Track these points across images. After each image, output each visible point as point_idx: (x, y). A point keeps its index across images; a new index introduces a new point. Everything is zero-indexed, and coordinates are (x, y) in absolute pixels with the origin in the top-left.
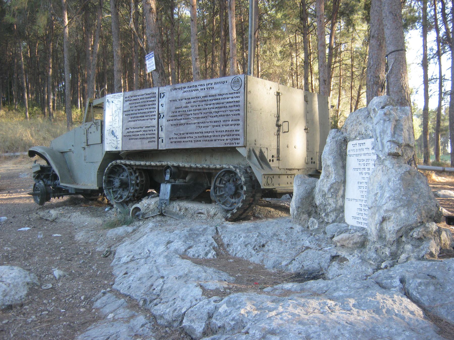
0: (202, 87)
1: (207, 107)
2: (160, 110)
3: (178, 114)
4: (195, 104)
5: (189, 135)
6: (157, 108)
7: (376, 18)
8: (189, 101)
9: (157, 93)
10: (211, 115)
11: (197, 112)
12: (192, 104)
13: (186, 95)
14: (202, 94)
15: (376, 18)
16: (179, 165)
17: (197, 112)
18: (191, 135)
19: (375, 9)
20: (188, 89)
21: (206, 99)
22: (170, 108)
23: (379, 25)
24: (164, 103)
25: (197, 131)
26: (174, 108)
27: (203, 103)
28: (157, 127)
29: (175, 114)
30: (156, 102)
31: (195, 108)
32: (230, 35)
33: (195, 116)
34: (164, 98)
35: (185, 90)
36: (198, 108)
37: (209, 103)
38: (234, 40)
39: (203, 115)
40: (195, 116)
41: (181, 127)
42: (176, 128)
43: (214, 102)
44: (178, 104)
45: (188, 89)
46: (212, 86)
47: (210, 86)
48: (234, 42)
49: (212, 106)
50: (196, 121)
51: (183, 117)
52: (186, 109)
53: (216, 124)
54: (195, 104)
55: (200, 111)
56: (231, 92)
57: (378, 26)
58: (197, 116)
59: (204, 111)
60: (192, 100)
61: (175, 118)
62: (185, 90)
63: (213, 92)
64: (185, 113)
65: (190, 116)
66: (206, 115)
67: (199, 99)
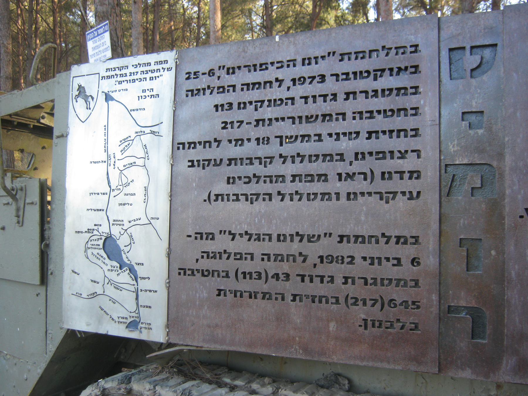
34: (487, 78)
38: (218, 31)
48: (217, 34)
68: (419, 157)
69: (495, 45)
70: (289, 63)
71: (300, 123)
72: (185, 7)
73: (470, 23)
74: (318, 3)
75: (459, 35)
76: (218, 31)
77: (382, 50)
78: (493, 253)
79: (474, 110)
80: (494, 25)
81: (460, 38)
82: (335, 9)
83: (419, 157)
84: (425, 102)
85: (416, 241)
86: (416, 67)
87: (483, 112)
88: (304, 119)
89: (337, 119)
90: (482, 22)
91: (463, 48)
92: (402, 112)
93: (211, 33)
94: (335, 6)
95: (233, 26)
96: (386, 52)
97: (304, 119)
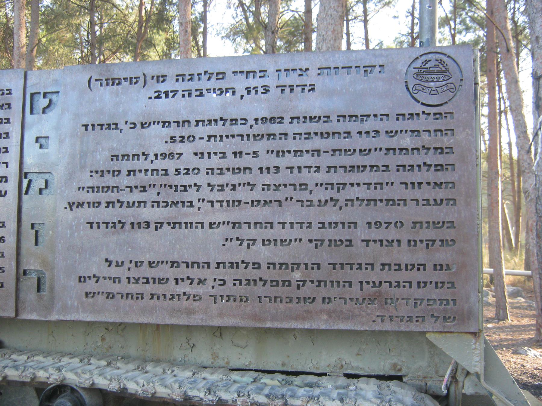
0: (252, 82)
1: (282, 162)
2: (28, 160)
3: (124, 181)
4: (213, 146)
5: (183, 272)
6: (14, 151)
7: (330, 27)
8: (185, 132)
9: (17, 94)
10: (305, 195)
11: (228, 178)
12: (202, 146)
13: (165, 107)
14: (257, 107)
15: (330, 27)
16: (125, 389)
17: (228, 178)
18: (196, 273)
19: (329, 13)
20: (180, 86)
21: (276, 128)
22: (84, 155)
23: (335, 40)
24: (52, 134)
25: (226, 258)
26: (107, 154)
27: (262, 146)
28: (12, 225)
29: (109, 180)
30: (14, 129)
31: (215, 162)
32: (16, 37)
33: (216, 196)
34: (52, 114)
35: (163, 87)
36: (230, 161)
37: (292, 145)
38: (22, 47)
39: (257, 195)
40: (216, 196)
41: (142, 237)
42: (115, 238)
43: (317, 143)
44: (127, 141)
45: (180, 86)
46: (307, 80)
47: (293, 79)
48: (21, 50)
49: (307, 160)
50: (221, 216)
51: (151, 195)
52: (170, 165)
53: (330, 234)
54: (213, 146)
55: (246, 177)
56: (406, 112)
57: (332, 42)
58: (228, 195)
59: (267, 179)
60: (203, 131)
61: (113, 196)
62: (163, 87)
63: (312, 104)
64: (164, 180)
65: (192, 195)
66: (280, 195)
67: (237, 129)
68: (7, 167)
69: (58, 92)
70: (177, 78)
71: (248, 140)
72: (9, 16)
73: (45, 77)
74: (144, 25)
75: (37, 84)
76: (22, 47)
77: (205, 75)
78: (51, 232)
79: (43, 136)
80: (59, 79)
81: (38, 86)
82: (166, 31)
83: (7, 167)
84: (13, 129)
85: (3, 225)
86: (9, 105)
87: (48, 137)
88: (251, 137)
89: (280, 139)
90: (52, 76)
91: (39, 93)
92: (336, 135)
93: (15, 49)
94: (166, 28)
95: (61, 40)
96: (208, 76)
97: (251, 137)
